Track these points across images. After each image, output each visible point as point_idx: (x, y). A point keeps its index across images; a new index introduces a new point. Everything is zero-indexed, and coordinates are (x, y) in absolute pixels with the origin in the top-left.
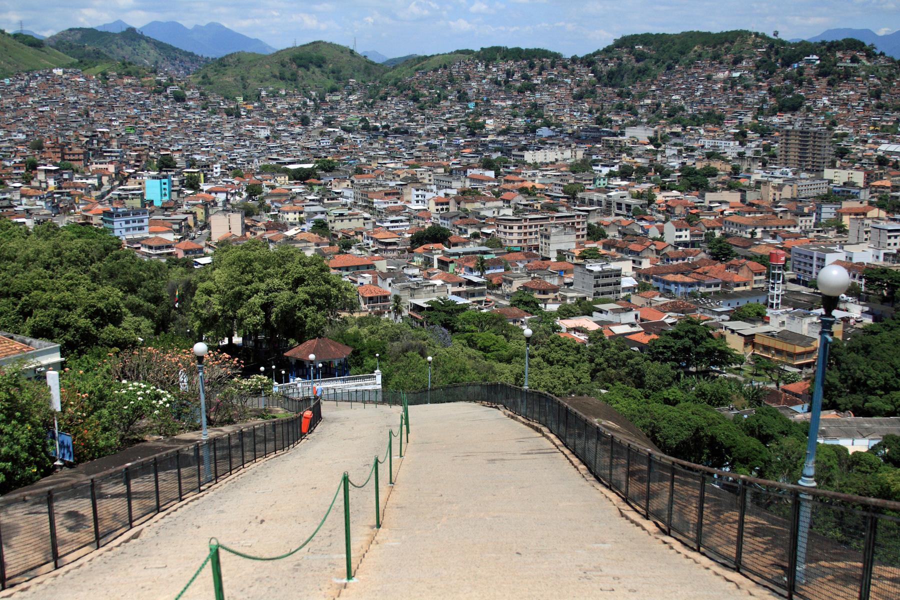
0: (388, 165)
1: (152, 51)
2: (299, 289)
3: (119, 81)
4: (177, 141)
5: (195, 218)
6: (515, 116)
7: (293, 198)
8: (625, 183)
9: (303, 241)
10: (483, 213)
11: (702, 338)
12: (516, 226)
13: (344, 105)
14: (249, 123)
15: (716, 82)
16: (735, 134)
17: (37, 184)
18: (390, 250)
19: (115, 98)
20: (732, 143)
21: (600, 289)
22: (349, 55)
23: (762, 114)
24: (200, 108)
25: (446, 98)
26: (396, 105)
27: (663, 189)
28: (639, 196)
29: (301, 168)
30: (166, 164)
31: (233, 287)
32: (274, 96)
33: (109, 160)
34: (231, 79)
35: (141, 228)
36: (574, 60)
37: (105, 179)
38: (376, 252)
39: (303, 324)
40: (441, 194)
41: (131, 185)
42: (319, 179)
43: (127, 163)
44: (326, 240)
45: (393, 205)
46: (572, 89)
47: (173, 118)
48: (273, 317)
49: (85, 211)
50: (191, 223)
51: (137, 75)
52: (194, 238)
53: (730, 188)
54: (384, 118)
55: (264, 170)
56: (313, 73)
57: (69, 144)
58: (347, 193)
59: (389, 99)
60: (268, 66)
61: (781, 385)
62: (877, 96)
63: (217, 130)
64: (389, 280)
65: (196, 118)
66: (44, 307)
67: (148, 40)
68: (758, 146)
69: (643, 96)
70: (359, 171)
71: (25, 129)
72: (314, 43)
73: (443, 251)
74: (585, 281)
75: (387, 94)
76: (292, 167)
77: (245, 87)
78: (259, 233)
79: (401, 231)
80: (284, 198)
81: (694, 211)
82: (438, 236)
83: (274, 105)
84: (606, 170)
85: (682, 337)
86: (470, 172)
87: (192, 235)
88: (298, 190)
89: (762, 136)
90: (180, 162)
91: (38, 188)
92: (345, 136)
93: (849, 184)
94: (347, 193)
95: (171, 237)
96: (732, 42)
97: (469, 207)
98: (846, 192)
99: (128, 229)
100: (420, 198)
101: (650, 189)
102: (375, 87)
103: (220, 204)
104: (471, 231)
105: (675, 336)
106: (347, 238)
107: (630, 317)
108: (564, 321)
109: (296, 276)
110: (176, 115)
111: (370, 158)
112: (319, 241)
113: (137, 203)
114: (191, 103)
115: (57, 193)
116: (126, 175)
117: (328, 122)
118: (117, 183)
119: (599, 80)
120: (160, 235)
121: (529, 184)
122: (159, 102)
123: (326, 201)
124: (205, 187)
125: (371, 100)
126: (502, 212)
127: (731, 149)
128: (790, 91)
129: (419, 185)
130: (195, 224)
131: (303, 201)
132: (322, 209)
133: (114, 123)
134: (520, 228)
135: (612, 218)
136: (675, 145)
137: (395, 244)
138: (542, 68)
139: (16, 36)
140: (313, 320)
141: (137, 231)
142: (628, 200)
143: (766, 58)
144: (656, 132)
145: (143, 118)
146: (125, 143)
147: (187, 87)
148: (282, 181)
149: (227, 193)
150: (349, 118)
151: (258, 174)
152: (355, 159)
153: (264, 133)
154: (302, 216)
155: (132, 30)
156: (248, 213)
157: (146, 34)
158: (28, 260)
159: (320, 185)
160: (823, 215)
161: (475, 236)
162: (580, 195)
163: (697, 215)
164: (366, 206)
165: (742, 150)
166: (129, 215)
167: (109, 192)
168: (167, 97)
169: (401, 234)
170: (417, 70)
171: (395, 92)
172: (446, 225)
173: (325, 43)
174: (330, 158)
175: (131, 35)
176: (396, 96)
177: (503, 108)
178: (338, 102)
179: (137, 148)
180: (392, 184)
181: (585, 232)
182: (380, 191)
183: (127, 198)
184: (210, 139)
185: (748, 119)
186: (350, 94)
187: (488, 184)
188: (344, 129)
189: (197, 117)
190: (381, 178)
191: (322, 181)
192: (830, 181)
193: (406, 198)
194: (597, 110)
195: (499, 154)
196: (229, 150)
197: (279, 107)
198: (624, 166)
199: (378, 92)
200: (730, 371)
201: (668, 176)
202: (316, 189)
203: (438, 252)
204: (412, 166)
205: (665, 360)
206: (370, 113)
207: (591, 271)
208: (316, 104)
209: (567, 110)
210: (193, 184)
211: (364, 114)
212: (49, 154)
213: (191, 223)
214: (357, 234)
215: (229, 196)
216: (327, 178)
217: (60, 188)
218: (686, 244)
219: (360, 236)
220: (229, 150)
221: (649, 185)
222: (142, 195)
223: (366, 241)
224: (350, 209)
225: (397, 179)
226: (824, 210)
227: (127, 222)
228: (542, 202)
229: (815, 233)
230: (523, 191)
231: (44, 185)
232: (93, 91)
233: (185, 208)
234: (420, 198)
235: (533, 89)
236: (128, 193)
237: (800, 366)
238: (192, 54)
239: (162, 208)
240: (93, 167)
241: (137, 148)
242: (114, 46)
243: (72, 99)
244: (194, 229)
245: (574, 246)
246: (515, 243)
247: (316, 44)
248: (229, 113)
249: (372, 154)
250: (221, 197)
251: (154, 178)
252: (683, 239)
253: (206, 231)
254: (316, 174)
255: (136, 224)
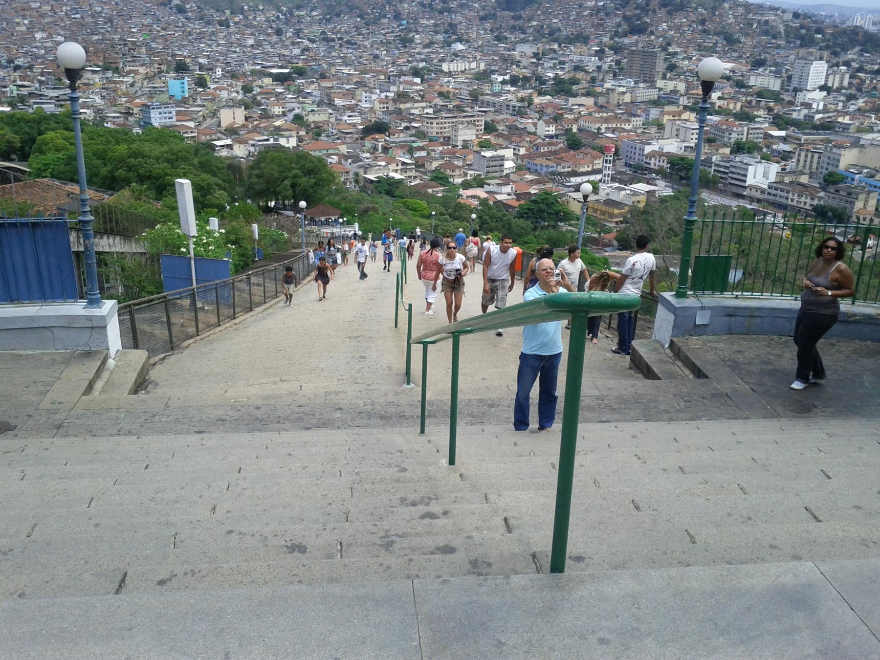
7: (278, 95)
8: (513, 89)
10: (412, 111)
11: (553, 203)
12: (435, 122)
15: (586, 8)
16: (596, 51)
20: (593, 58)
21: (491, 169)
25: (385, 17)
27: (540, 94)
28: (522, 100)
30: (181, 68)
40: (383, 95)
46: (478, 12)
53: (588, 94)
62: (703, 22)
64: (350, 161)
65: (197, 27)
68: (612, 61)
69: (530, 19)
70: (323, 76)
74: (545, 66)
81: (560, 112)
82: (379, 128)
83: (255, 18)
84: (500, 79)
85: (539, 203)
86: (402, 79)
89: (615, 53)
92: (311, 46)
93: (675, 92)
94: (315, 93)
97: (402, 106)
98: (670, 99)
101: (531, 95)
104: (404, 125)
105: (535, 202)
107: (507, 189)
108: (465, 191)
114: (190, 14)
117: (297, 34)
120: (184, 123)
127: (592, 63)
128: (640, 18)
129: (366, 89)
134: (438, 124)
135: (501, 117)
136: (552, 59)
142: (514, 103)
144: (538, 49)
148: (268, 81)
153: (251, 42)
161: (407, 128)
162: (481, 98)
163: (562, 115)
165: (600, 64)
172: (387, 119)
177: (427, 26)
180: (347, 87)
184: (209, 46)
185: (606, 40)
186: (312, 10)
187: (415, 88)
188: (309, 40)
192: (660, 89)
194: (497, 29)
195: (424, 63)
196: (225, 55)
198: (514, 76)
200: (569, 225)
201: (544, 84)
203: (381, 140)
205: (527, 219)
208: (286, 19)
209: (475, 28)
218: (551, 137)
221: (530, 91)
227: (160, 113)
229: (642, 130)
235: (450, 11)
245: (474, 137)
246: (434, 134)
252: (550, 133)
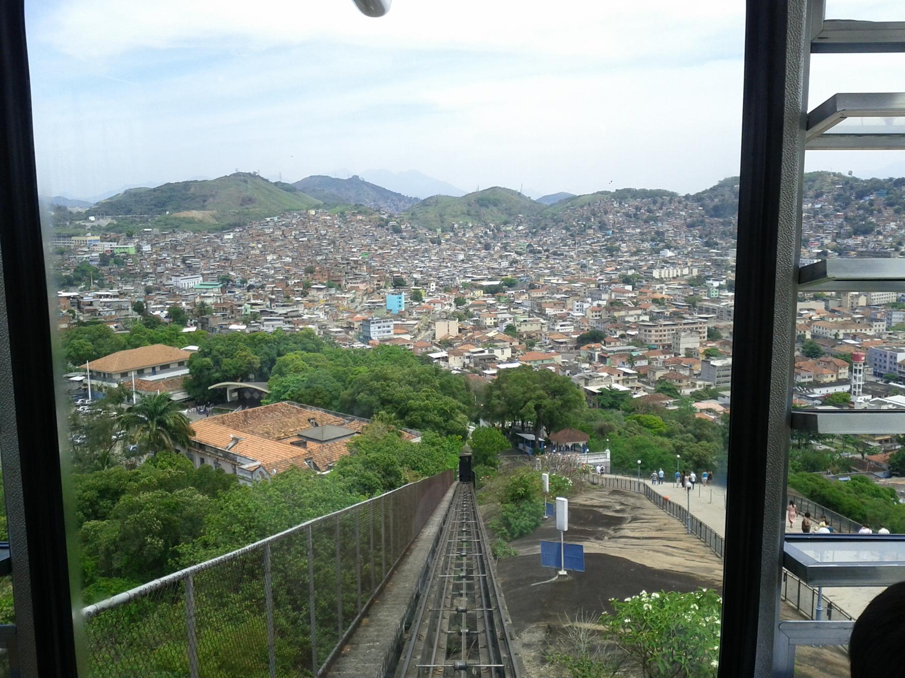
6: (643, 241)
10: (627, 319)
23: (840, 237)
25: (590, 228)
36: (687, 197)
61: (866, 455)
65: (410, 245)
71: (291, 254)
73: (602, 349)
76: (485, 283)
82: (595, 337)
83: (464, 235)
84: (716, 284)
88: (491, 302)
96: (813, 181)
97: (616, 314)
104: (619, 333)
110: (396, 243)
117: (505, 247)
119: (707, 212)
121: (658, 296)
126: (641, 318)
133: (354, 250)
134: (656, 331)
138: (663, 204)
139: (276, 184)
143: (842, 192)
160: (893, 320)
161: (622, 336)
162: (698, 304)
177: (633, 235)
181: (706, 334)
184: (422, 262)
186: (518, 226)
188: (517, 253)
194: (706, 236)
203: (598, 349)
207: (715, 366)
210: (417, 297)
226: (894, 316)
228: (671, 310)
230: (655, 301)
235: (656, 220)
237: (880, 442)
246: (653, 342)
247: (494, 189)
255: (386, 329)
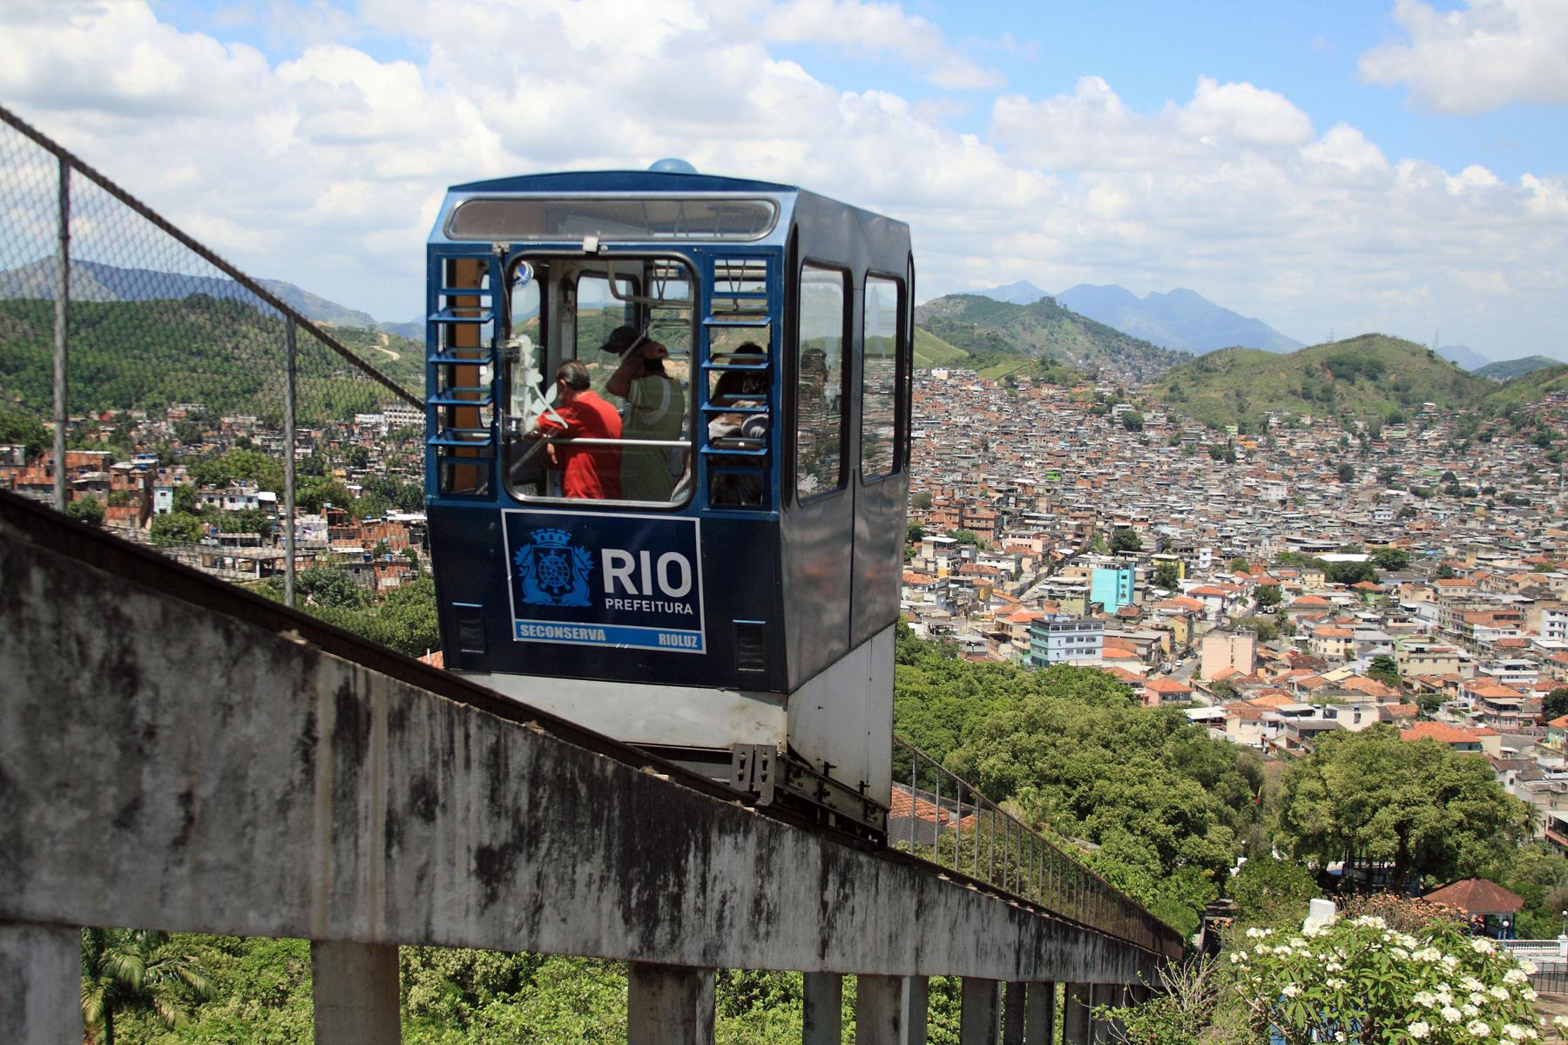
0: (1495, 563)
1: (1080, 338)
2: (1451, 804)
3: (1034, 391)
4: (1130, 499)
5: (1172, 638)
9: (1356, 692)
13: (1412, 446)
14: (1250, 474)
17: (921, 565)
18: (1506, 719)
19: (1030, 422)
22: (1425, 359)
24: (1166, 443)
26: (1507, 451)
29: (1349, 563)
30: (1124, 544)
31: (1351, 794)
32: (1291, 427)
33: (1034, 531)
34: (1219, 395)
35: (1090, 651)
37: (1026, 563)
38: (1479, 719)
39: (1455, 857)
41: (1069, 575)
42: (1377, 582)
43: (1062, 538)
44: (1394, 692)
45: (1508, 636)
47: (1124, 459)
48: (1412, 843)
49: (1000, 615)
50: (1166, 646)
51: (1064, 381)
52: (1170, 672)
54: (1485, 474)
55: (1283, 560)
56: (1362, 389)
57: (971, 501)
58: (1427, 610)
59: (1495, 439)
60: (1282, 375)
63: (1197, 484)
65: (1161, 459)
66: (1112, 803)
67: (1074, 318)
70: (1446, 573)
72: (1365, 337)
75: (1491, 430)
76: (1330, 557)
77: (1241, 409)
78: (1281, 672)
79: (1522, 685)
80: (1319, 614)
83: (1291, 442)
87: (1168, 666)
88: (1343, 601)
90: (1149, 543)
91: (924, 572)
94: (1427, 610)
95: (1136, 668)
99: (1069, 651)
100: (1556, 628)
102: (1470, 418)
103: (1212, 617)
106: (1429, 690)
109: (1447, 784)
110: (1128, 454)
111: (1463, 549)
112: (1383, 693)
113: (1078, 607)
114: (1151, 434)
115: (953, 582)
116: (1060, 557)
117: (1386, 478)
118: (1044, 570)
120: (1118, 664)
122: (1098, 430)
123: (1390, 623)
124: (1186, 585)
125: (1462, 442)
129: (1554, 605)
130: (1173, 649)
131: (1351, 621)
132: (1385, 637)
133: (1026, 464)
137: (1514, 708)
140: (1470, 852)
141: (1084, 656)
145: (1074, 456)
146: (1058, 505)
147: (1145, 405)
148: (1314, 583)
149: (1223, 598)
150: (1422, 470)
151: (1273, 567)
152: (1435, 548)
153: (1277, 493)
154: (1350, 646)
155: (1048, 302)
156: (1262, 635)
157: (1071, 309)
158: (1084, 736)
159: (1379, 593)
164: (1459, 636)
166: (1073, 628)
167: (1031, 584)
168: (1111, 422)
169: (1523, 690)
170: (1547, 390)
171: (1506, 428)
173: (1384, 337)
174: (1392, 546)
175: (1048, 310)
176: (1508, 435)
178: (1402, 442)
179: (1077, 513)
180: (1507, 599)
182: (1487, 612)
183: (1063, 598)
184: (1186, 498)
186: (1424, 428)
188: (1415, 492)
189: (1163, 459)
190: (1483, 587)
191: (1382, 587)
193: (1531, 625)
196: (1219, 520)
197: (1299, 446)
199: (1475, 426)
202: (1372, 598)
204: (1541, 568)
206: (1461, 464)
208: (1363, 445)
210: (1167, 580)
211: (1448, 465)
212: (940, 515)
213: (1166, 646)
214: (1446, 685)
215: (1226, 604)
216: (1390, 581)
217: (956, 573)
219: (1452, 690)
220: (1219, 520)
222: (1088, 593)
223: (1463, 699)
224: (1432, 640)
225: (1514, 589)
227: (1070, 640)
231: (931, 567)
232: (994, 408)
233: (1155, 620)
234: (1556, 628)
236: (1064, 588)
238: (1146, 345)
239: (1118, 617)
240: (1008, 542)
241: (1077, 513)
242: (1019, 328)
243: (962, 421)
244: (1170, 656)
247: (1367, 338)
248: (1215, 455)
249: (1467, 541)
250: (1214, 605)
251: (1107, 567)
253: (1188, 660)
254: (1371, 573)
255: (1084, 644)
